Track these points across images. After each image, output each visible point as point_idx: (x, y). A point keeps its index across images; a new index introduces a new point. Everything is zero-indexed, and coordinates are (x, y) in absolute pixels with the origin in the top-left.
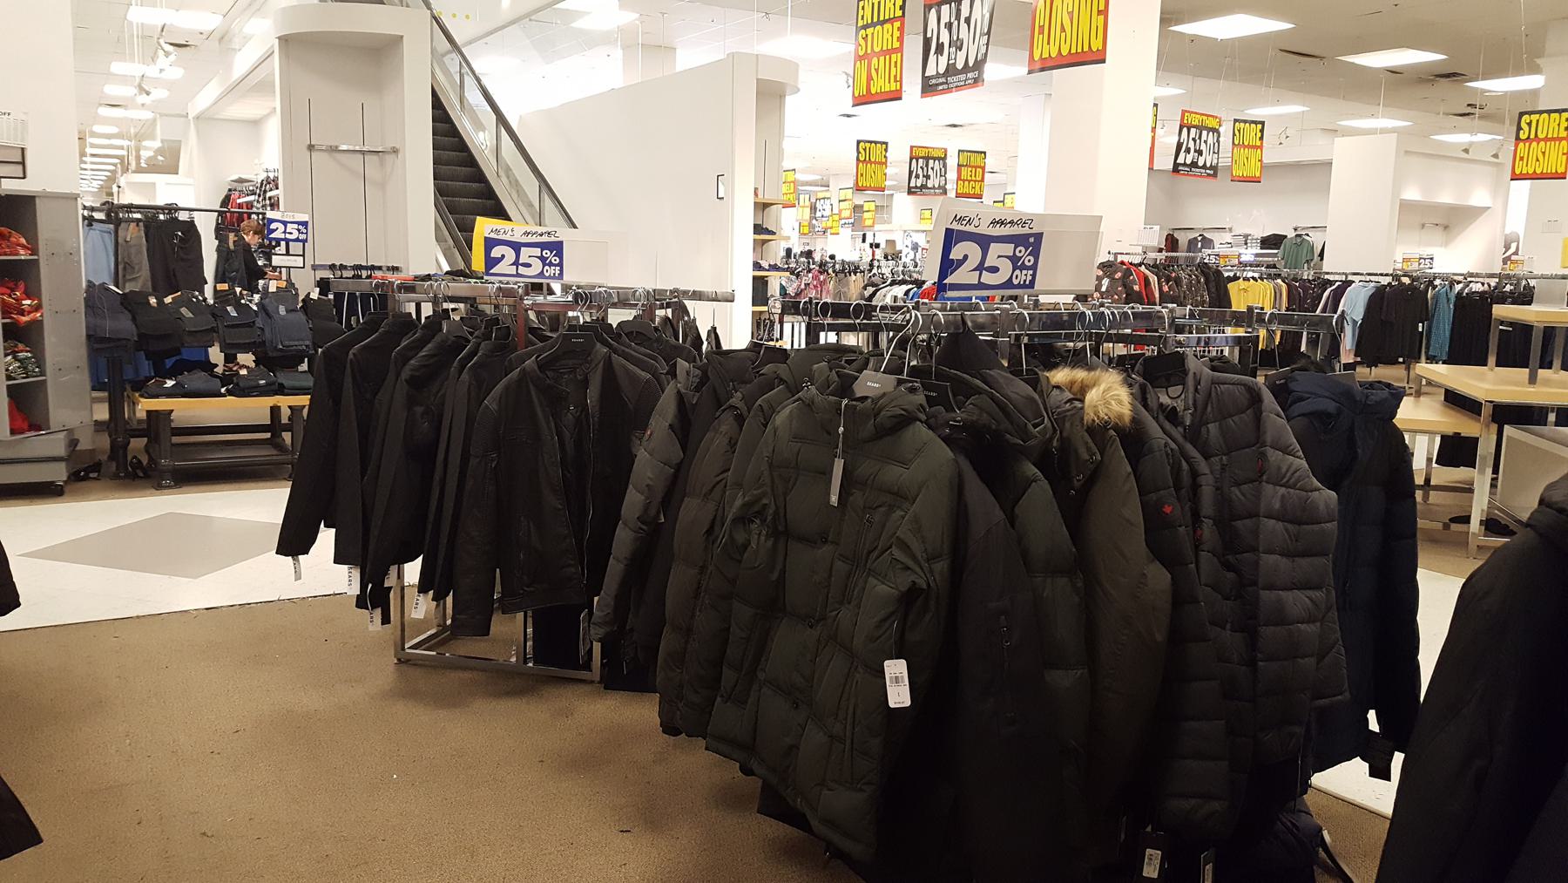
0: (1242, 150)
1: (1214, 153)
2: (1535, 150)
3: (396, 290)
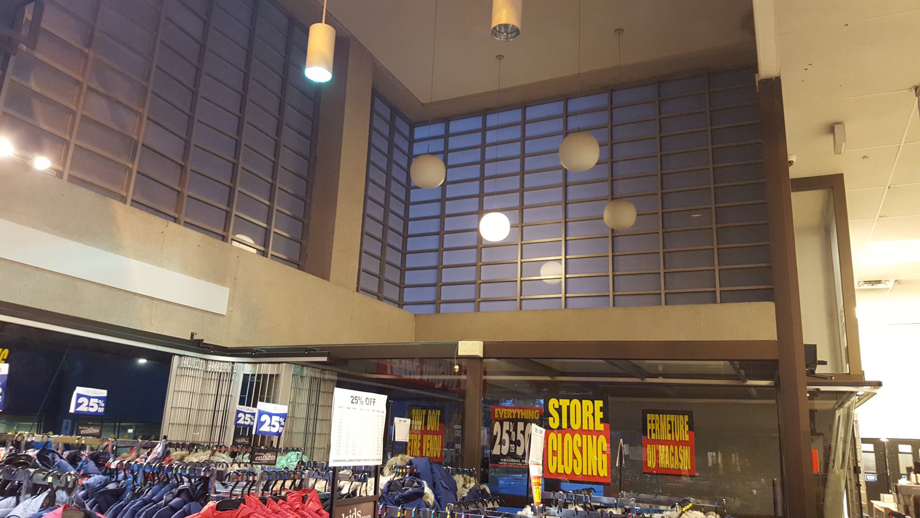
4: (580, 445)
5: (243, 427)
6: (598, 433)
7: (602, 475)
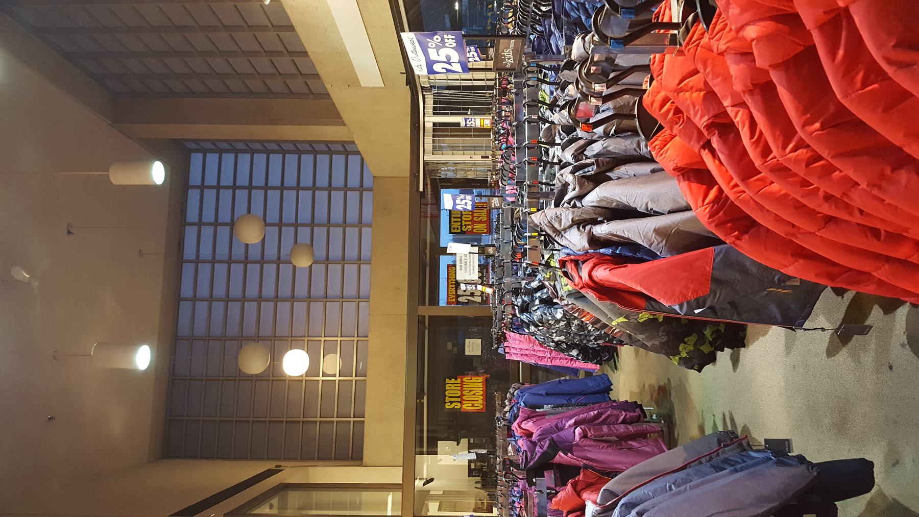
2: (468, 396)
4: (468, 391)
6: (462, 382)
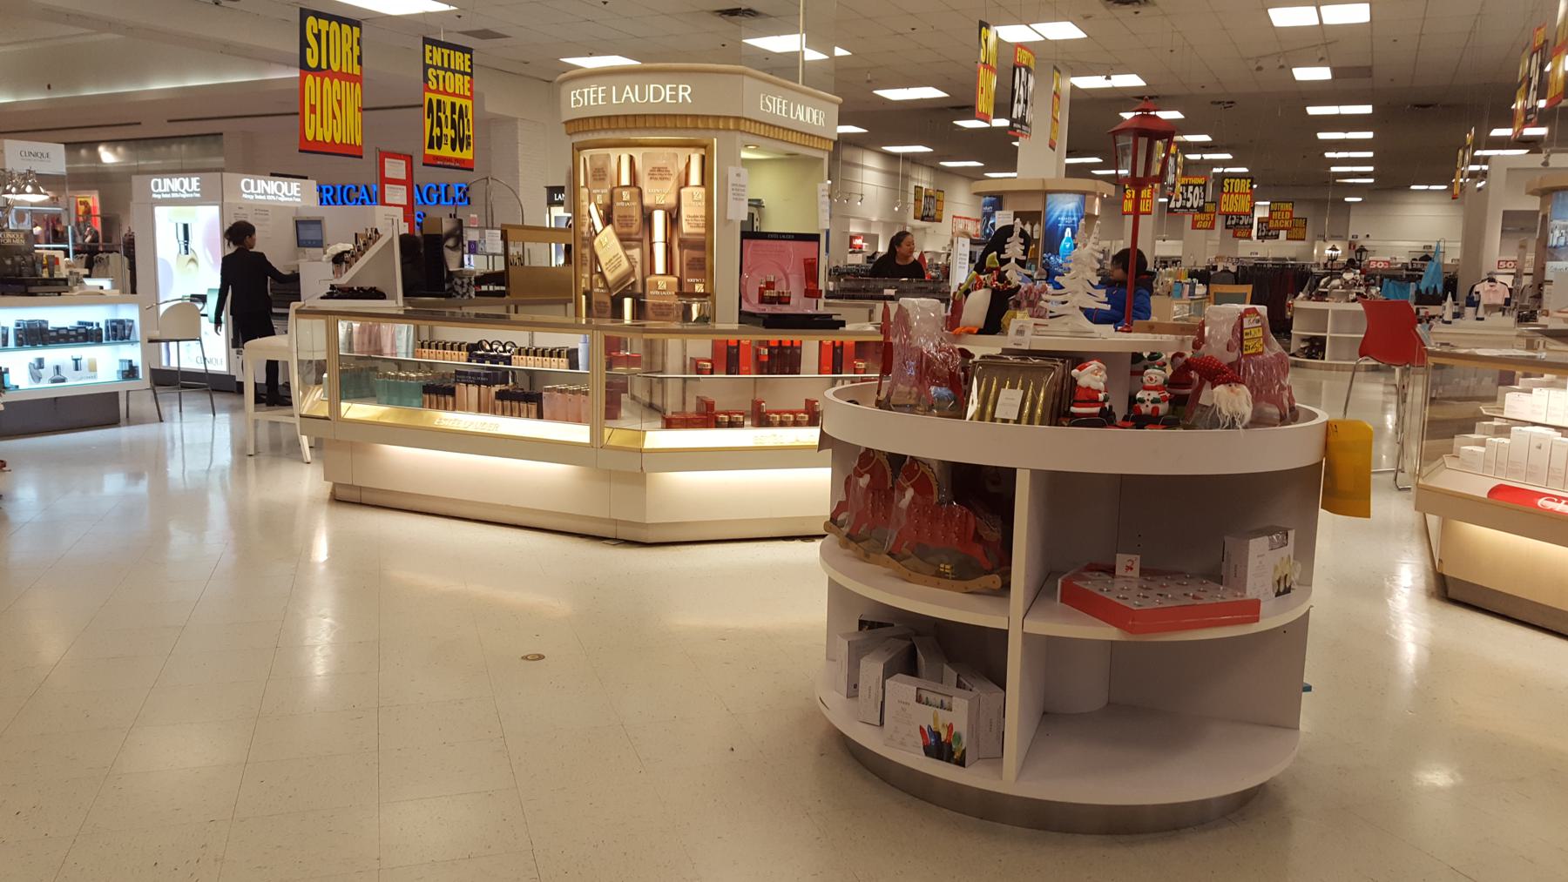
0: (327, 80)
1: (1200, 198)
3: (473, 283)
4: (339, 98)
5: (101, 341)
7: (263, 181)
